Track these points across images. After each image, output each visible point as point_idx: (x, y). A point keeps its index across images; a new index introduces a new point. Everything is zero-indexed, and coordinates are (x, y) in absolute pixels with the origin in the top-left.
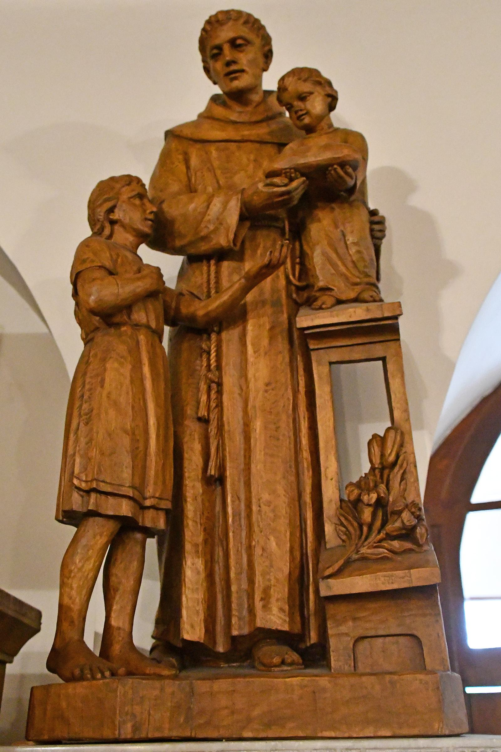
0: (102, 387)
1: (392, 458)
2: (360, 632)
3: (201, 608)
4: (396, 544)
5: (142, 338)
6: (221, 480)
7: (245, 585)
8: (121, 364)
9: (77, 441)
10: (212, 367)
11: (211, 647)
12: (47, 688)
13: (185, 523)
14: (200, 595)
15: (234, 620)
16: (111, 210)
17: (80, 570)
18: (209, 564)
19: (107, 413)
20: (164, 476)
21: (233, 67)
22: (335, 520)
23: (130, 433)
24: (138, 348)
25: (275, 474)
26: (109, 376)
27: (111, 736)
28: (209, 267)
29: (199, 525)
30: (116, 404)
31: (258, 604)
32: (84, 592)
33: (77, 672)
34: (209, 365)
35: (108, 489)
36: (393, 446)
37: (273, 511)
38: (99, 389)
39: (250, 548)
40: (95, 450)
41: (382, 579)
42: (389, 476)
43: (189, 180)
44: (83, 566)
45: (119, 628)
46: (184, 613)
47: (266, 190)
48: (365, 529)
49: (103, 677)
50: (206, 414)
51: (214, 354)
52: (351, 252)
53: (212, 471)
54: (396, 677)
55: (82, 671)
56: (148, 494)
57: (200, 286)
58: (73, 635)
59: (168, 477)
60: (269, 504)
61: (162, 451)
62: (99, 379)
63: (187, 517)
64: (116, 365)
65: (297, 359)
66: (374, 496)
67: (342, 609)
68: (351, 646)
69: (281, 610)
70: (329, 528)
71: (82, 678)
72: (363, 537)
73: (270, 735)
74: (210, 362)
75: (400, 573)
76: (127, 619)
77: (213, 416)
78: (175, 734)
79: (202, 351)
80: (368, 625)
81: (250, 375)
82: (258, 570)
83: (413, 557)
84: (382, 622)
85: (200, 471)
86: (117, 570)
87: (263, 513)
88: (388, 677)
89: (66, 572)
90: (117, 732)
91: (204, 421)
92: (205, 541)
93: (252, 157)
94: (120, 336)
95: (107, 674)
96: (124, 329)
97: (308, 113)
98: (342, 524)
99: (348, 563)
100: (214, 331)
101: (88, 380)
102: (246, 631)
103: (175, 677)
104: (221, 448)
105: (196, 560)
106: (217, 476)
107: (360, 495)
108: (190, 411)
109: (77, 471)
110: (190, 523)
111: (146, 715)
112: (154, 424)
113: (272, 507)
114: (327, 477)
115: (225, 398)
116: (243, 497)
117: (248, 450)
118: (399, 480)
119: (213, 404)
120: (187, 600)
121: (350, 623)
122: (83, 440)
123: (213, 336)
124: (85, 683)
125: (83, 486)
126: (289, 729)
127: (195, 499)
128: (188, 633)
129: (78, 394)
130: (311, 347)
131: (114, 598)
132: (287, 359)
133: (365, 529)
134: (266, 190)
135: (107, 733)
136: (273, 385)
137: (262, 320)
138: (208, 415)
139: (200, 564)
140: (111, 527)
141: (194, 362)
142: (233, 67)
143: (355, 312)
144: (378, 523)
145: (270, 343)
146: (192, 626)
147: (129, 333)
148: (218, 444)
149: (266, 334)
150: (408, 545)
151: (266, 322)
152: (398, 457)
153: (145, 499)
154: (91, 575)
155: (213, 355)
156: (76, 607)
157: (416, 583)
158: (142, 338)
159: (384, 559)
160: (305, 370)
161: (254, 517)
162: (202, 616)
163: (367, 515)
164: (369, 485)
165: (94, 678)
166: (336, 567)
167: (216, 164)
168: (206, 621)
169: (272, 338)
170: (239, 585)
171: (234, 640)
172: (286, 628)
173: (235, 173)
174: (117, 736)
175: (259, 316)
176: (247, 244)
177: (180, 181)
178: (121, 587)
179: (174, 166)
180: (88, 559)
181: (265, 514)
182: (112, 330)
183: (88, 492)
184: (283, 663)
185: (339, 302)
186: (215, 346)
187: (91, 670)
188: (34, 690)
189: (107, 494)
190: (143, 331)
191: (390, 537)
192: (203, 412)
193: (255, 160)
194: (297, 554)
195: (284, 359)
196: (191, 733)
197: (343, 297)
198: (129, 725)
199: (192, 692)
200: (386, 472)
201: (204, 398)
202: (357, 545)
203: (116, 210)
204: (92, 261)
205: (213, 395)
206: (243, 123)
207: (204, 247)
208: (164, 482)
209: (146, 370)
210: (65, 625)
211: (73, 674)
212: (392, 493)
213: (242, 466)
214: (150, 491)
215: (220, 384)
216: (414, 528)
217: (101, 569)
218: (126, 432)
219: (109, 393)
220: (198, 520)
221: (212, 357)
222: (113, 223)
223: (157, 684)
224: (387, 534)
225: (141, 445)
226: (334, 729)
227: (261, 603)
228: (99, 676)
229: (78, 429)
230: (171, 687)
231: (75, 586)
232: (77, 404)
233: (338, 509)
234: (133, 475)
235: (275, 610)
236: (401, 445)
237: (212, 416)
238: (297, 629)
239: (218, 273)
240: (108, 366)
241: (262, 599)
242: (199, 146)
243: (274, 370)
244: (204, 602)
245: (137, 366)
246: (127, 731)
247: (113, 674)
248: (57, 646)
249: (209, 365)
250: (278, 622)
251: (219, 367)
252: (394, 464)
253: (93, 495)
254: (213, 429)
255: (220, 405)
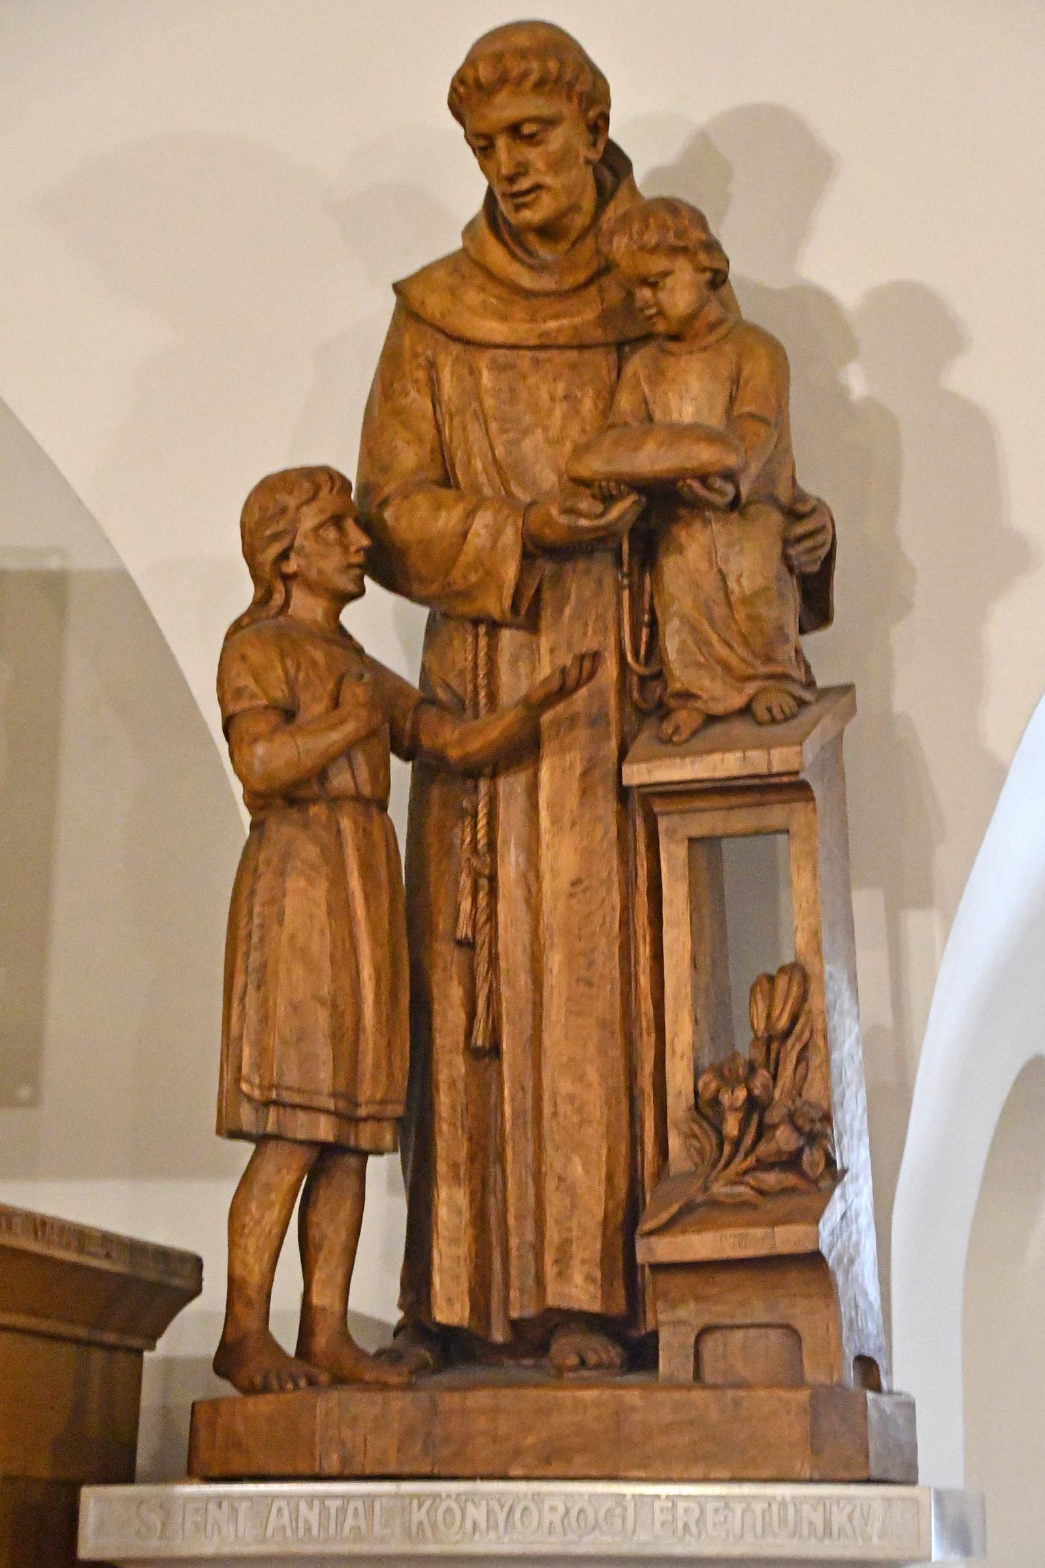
0: (281, 922)
1: (783, 1023)
2: (706, 1319)
3: (464, 1271)
4: (771, 1179)
5: (346, 824)
6: (494, 1050)
7: (530, 1236)
8: (310, 881)
9: (243, 1015)
10: (480, 846)
11: (481, 1333)
12: (215, 1404)
13: (437, 1126)
14: (463, 1249)
15: (514, 1294)
16: (284, 556)
17: (258, 1222)
18: (479, 1195)
19: (289, 970)
20: (390, 1064)
21: (524, 184)
22: (684, 1127)
23: (329, 1004)
24: (340, 846)
25: (585, 1046)
26: (291, 904)
27: (308, 1471)
28: (476, 636)
29: (460, 1131)
30: (303, 954)
31: (550, 1271)
32: (266, 1257)
33: (258, 1380)
34: (474, 841)
35: (297, 1099)
36: (785, 1003)
37: (579, 1111)
38: (275, 927)
39: (538, 1177)
40: (272, 1036)
41: (731, 1240)
42: (779, 1052)
43: (439, 430)
44: (262, 1218)
45: (324, 1309)
46: (436, 1279)
47: (563, 520)
48: (727, 1149)
49: (296, 1387)
50: (470, 935)
51: (485, 811)
52: (737, 616)
53: (479, 1041)
54: (742, 1393)
55: (266, 1377)
56: (362, 1098)
57: (462, 673)
58: (250, 1322)
59: (397, 1063)
60: (572, 1098)
61: (387, 1023)
62: (275, 909)
63: (441, 1118)
64: (302, 883)
65: (634, 824)
66: (742, 1094)
67: (678, 1282)
68: (692, 1340)
69: (589, 1278)
70: (674, 1142)
71: (265, 1389)
72: (722, 1162)
73: (551, 1473)
74: (476, 836)
75: (759, 1232)
76: (338, 1293)
77: (482, 938)
78: (407, 1469)
79: (463, 812)
80: (718, 1308)
81: (544, 866)
82: (551, 1212)
83: (794, 1202)
84: (742, 1304)
85: (462, 1038)
86: (320, 1214)
87: (561, 1119)
88: (730, 1393)
89: (237, 1225)
90: (317, 1466)
91: (467, 945)
92: (472, 1158)
93: (560, 388)
94: (306, 825)
95: (303, 1383)
96: (314, 810)
97: (661, 313)
98: (695, 1136)
99: (688, 1208)
100: (484, 775)
101: (257, 909)
102: (531, 1311)
103: (408, 1387)
104: (493, 998)
105: (455, 1190)
106: (487, 1046)
107: (718, 1091)
108: (442, 925)
109: (245, 1069)
110: (445, 1127)
111: (359, 1441)
112: (370, 979)
113: (577, 1105)
114: (674, 1052)
115: (502, 908)
116: (529, 1085)
117: (538, 1005)
118: (794, 1061)
119: (482, 918)
120: (441, 1257)
121: (692, 1305)
122: (251, 1012)
123: (483, 786)
124: (270, 1397)
125: (257, 1094)
126: (578, 1464)
127: (453, 1084)
128: (442, 1312)
129: (242, 933)
130: (656, 809)
131: (316, 1260)
132: (613, 832)
133: (727, 1149)
134: (563, 520)
135: (303, 1467)
136: (586, 884)
137: (568, 757)
138: (474, 936)
139: (462, 1197)
140: (303, 1156)
141: (452, 828)
142: (524, 184)
143: (723, 760)
144: (748, 1140)
145: (582, 804)
146: (450, 1301)
147: (324, 818)
148: (490, 991)
149: (575, 785)
150: (791, 1179)
151: (575, 759)
152: (794, 1020)
153: (357, 1105)
154: (276, 1231)
155: (482, 822)
156: (255, 1278)
157: (782, 1248)
158: (346, 824)
159: (742, 1205)
160: (648, 847)
161: (546, 1124)
162: (465, 1286)
163: (731, 1126)
164: (737, 1073)
165: (282, 1389)
166: (665, 1216)
167: (489, 402)
168: (472, 1292)
169: (585, 792)
170: (521, 1236)
171: (515, 1326)
172: (596, 1307)
173: (526, 432)
174: (317, 1470)
175: (563, 751)
176: (547, 595)
177: (421, 440)
178: (326, 1244)
179: (409, 400)
180: (271, 1205)
181: (565, 1118)
182: (295, 815)
183: (267, 1103)
184: (583, 1363)
185: (712, 719)
186: (485, 805)
187: (279, 1376)
188: (197, 1408)
189: (294, 1107)
190: (349, 806)
191: (762, 1165)
192: (464, 930)
193: (566, 397)
194: (622, 1184)
195: (606, 833)
196: (832, 1378)
197: (718, 708)
198: (335, 1457)
199: (434, 1410)
200: (775, 1046)
201: (466, 905)
202: (707, 1177)
203: (293, 556)
204: (253, 696)
205: (482, 896)
206: (547, 294)
207: (462, 608)
208: (390, 1075)
209: (355, 883)
210: (239, 1308)
211: (252, 1382)
212: (780, 1084)
213: (529, 1032)
214: (366, 1091)
215: (493, 879)
216: (799, 1152)
217: (294, 1210)
218: (321, 1001)
219: (293, 937)
220: (459, 1124)
221: (480, 825)
222: (287, 578)
223: (378, 1397)
224: (758, 1160)
225: (348, 1021)
226: (644, 1466)
227: (555, 1269)
228: (290, 1386)
229: (244, 993)
230: (399, 1402)
231: (251, 1249)
232: (242, 949)
233: (690, 1109)
234: (335, 1073)
235: (578, 1278)
236: (804, 998)
237: (480, 939)
238: (619, 1305)
239: (492, 650)
240: (289, 885)
241: (556, 1261)
242: (456, 348)
243: (587, 855)
244: (468, 1261)
245: (338, 880)
246: (333, 1463)
247: (312, 1382)
248: (230, 1338)
249: (474, 841)
250: (583, 1297)
251: (492, 846)
252: (787, 1033)
253: (273, 1112)
254: (483, 955)
255: (492, 917)
